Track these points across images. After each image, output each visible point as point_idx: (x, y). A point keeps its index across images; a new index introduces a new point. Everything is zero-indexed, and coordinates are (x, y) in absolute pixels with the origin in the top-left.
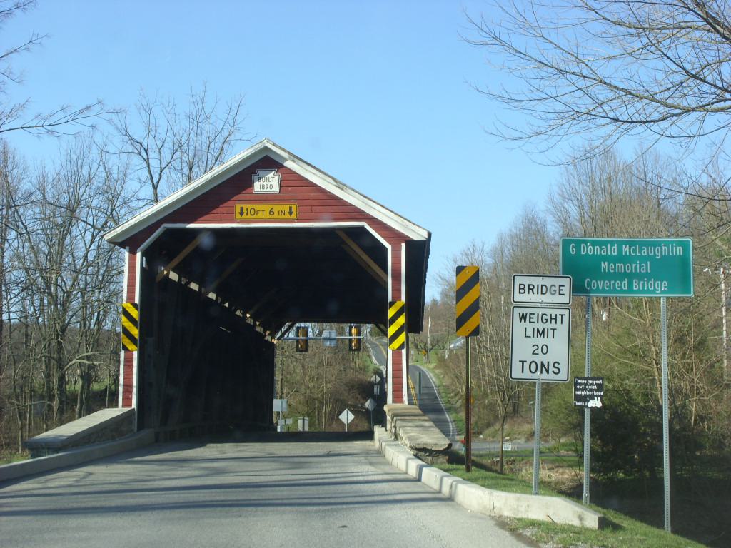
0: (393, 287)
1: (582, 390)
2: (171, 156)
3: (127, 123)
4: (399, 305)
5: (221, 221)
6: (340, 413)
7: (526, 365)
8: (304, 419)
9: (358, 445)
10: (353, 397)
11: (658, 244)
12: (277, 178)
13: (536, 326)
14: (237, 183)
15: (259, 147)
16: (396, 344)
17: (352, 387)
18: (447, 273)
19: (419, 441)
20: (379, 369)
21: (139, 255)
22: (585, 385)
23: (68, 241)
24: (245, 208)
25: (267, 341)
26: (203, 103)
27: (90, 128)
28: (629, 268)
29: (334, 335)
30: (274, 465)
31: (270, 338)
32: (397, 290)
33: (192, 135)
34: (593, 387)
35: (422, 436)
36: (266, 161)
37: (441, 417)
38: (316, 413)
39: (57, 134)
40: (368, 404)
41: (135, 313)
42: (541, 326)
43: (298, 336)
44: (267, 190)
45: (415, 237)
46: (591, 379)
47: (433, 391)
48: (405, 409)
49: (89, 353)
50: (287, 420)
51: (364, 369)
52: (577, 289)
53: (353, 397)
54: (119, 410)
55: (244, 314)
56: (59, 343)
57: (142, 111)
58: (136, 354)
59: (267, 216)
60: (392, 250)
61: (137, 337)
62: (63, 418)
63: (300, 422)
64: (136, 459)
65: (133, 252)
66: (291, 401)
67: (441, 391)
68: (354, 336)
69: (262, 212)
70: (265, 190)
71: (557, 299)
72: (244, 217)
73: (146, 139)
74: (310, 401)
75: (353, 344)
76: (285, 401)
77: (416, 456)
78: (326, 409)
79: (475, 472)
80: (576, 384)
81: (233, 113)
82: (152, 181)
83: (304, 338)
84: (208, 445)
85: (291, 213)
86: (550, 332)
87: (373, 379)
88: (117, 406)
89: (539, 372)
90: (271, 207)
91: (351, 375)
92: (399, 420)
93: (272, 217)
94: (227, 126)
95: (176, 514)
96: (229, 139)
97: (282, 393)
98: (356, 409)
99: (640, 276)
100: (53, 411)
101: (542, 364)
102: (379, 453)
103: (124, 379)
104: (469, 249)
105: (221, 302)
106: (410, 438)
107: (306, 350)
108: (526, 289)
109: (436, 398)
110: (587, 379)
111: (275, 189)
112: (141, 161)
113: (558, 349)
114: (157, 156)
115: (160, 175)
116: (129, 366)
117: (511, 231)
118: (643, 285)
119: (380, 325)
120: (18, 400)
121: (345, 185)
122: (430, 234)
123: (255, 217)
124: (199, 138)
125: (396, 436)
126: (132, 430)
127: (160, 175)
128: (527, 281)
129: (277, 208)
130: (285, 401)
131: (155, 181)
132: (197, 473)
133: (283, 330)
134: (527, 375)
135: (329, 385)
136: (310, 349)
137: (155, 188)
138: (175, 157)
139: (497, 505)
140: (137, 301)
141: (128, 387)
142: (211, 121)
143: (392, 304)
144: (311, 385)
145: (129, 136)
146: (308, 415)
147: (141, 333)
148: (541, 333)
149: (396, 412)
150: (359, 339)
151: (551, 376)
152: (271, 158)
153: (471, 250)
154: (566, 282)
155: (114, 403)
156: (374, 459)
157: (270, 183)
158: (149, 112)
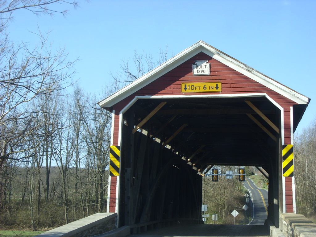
0: (285, 135)
3: (129, 67)
5: (172, 93)
6: (231, 211)
8: (215, 215)
10: (236, 204)
12: (208, 66)
14: (181, 70)
20: (247, 191)
21: (121, 115)
23: (105, 130)
24: (187, 85)
27: (73, 5)
36: (202, 56)
38: (220, 211)
39: (50, 12)
40: (244, 207)
41: (118, 152)
43: (213, 173)
44: (202, 74)
45: (300, 102)
48: (294, 217)
51: (241, 191)
54: (107, 214)
56: (101, 177)
57: (137, 62)
58: (118, 178)
59: (202, 90)
60: (284, 111)
61: (119, 167)
63: (213, 216)
65: (117, 114)
68: (241, 174)
69: (198, 88)
70: (200, 74)
72: (187, 91)
74: (217, 205)
83: (216, 174)
85: (217, 88)
87: (245, 195)
88: (106, 211)
92: (298, 226)
93: (205, 91)
98: (238, 209)
100: (98, 208)
105: (174, 151)
107: (217, 181)
111: (207, 72)
116: (113, 183)
117: (309, 127)
119: (259, 167)
120: (83, 203)
121: (252, 69)
122: (309, 100)
123: (194, 91)
126: (115, 227)
129: (208, 85)
140: (119, 144)
141: (113, 199)
143: (284, 146)
150: (244, 175)
152: (204, 53)
157: (204, 69)
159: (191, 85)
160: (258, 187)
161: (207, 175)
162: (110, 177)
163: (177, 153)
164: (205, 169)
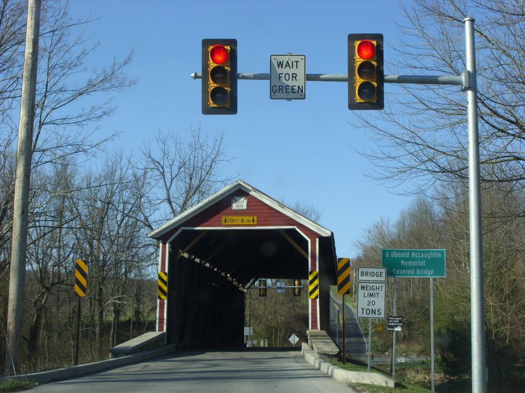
1: (392, 323)
2: (178, 170)
3: (151, 151)
4: (315, 273)
6: (290, 336)
7: (365, 311)
8: (264, 341)
9: (293, 353)
10: (299, 326)
11: (429, 252)
12: (246, 201)
13: (369, 292)
14: (221, 206)
15: (236, 184)
16: (313, 296)
17: (299, 319)
18: (363, 240)
19: (322, 350)
22: (393, 320)
24: (227, 218)
25: (240, 290)
26: (198, 137)
28: (415, 264)
29: (283, 285)
30: (244, 363)
31: (242, 288)
32: (314, 265)
33: (192, 157)
34: (397, 321)
35: (324, 347)
36: (239, 192)
37: (360, 340)
38: (274, 337)
41: (165, 278)
42: (372, 292)
43: (260, 286)
45: (324, 235)
46: (397, 317)
47: (355, 322)
49: (120, 296)
50: (253, 341)
52: (390, 274)
53: (299, 326)
55: (226, 275)
56: (101, 289)
57: (160, 143)
58: (166, 301)
59: (240, 223)
61: (166, 291)
62: (103, 340)
63: (262, 342)
64: (169, 359)
65: (164, 244)
66: (256, 329)
67: (361, 322)
68: (297, 286)
69: (237, 221)
71: (379, 279)
72: (227, 223)
73: (162, 160)
74: (269, 328)
75: (296, 291)
76: (251, 328)
77: (320, 358)
78: (281, 334)
79: (348, 364)
80: (389, 320)
81: (218, 143)
82: (166, 186)
83: (264, 287)
84: (207, 353)
85: (253, 221)
86: (376, 295)
89: (370, 314)
90: (243, 217)
91: (298, 311)
93: (243, 223)
94: (214, 151)
95: (197, 381)
96: (215, 160)
97: (250, 323)
99: (420, 268)
101: (372, 310)
102: (303, 357)
103: (159, 315)
104: (379, 224)
106: (318, 348)
108: (365, 274)
109: (358, 326)
110: (394, 317)
111: (245, 207)
112: (159, 173)
113: (380, 303)
114: (169, 170)
115: (171, 183)
118: (422, 272)
121: (284, 205)
124: (196, 159)
125: (312, 347)
127: (171, 183)
128: (365, 270)
129: (246, 218)
130: (251, 328)
131: (168, 186)
132: (203, 366)
133: (251, 281)
134: (365, 315)
135: (282, 318)
136: (267, 295)
137: (168, 191)
138: (181, 171)
139: (349, 377)
140: (167, 271)
142: (203, 148)
143: (311, 273)
144: (270, 318)
145: (151, 158)
146: (268, 338)
147: (168, 289)
148: (371, 295)
149: (312, 334)
151: (377, 316)
153: (381, 224)
154: (384, 271)
155: (153, 329)
156: (299, 360)
158: (164, 142)
159: (230, 218)
160: (338, 299)
161: (251, 289)
162: (158, 301)
163: (216, 269)
164: (247, 284)
